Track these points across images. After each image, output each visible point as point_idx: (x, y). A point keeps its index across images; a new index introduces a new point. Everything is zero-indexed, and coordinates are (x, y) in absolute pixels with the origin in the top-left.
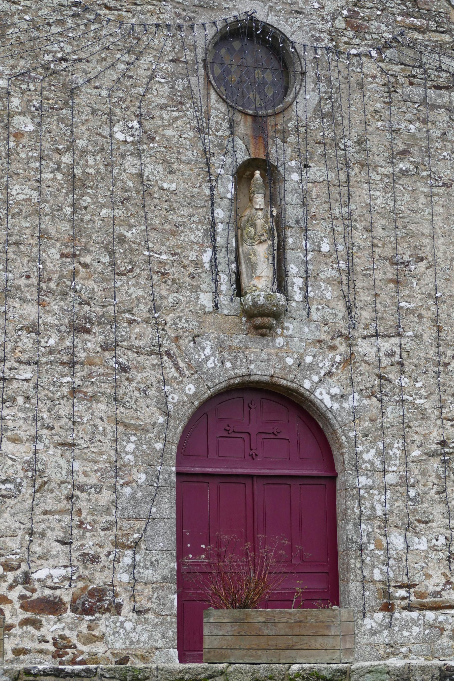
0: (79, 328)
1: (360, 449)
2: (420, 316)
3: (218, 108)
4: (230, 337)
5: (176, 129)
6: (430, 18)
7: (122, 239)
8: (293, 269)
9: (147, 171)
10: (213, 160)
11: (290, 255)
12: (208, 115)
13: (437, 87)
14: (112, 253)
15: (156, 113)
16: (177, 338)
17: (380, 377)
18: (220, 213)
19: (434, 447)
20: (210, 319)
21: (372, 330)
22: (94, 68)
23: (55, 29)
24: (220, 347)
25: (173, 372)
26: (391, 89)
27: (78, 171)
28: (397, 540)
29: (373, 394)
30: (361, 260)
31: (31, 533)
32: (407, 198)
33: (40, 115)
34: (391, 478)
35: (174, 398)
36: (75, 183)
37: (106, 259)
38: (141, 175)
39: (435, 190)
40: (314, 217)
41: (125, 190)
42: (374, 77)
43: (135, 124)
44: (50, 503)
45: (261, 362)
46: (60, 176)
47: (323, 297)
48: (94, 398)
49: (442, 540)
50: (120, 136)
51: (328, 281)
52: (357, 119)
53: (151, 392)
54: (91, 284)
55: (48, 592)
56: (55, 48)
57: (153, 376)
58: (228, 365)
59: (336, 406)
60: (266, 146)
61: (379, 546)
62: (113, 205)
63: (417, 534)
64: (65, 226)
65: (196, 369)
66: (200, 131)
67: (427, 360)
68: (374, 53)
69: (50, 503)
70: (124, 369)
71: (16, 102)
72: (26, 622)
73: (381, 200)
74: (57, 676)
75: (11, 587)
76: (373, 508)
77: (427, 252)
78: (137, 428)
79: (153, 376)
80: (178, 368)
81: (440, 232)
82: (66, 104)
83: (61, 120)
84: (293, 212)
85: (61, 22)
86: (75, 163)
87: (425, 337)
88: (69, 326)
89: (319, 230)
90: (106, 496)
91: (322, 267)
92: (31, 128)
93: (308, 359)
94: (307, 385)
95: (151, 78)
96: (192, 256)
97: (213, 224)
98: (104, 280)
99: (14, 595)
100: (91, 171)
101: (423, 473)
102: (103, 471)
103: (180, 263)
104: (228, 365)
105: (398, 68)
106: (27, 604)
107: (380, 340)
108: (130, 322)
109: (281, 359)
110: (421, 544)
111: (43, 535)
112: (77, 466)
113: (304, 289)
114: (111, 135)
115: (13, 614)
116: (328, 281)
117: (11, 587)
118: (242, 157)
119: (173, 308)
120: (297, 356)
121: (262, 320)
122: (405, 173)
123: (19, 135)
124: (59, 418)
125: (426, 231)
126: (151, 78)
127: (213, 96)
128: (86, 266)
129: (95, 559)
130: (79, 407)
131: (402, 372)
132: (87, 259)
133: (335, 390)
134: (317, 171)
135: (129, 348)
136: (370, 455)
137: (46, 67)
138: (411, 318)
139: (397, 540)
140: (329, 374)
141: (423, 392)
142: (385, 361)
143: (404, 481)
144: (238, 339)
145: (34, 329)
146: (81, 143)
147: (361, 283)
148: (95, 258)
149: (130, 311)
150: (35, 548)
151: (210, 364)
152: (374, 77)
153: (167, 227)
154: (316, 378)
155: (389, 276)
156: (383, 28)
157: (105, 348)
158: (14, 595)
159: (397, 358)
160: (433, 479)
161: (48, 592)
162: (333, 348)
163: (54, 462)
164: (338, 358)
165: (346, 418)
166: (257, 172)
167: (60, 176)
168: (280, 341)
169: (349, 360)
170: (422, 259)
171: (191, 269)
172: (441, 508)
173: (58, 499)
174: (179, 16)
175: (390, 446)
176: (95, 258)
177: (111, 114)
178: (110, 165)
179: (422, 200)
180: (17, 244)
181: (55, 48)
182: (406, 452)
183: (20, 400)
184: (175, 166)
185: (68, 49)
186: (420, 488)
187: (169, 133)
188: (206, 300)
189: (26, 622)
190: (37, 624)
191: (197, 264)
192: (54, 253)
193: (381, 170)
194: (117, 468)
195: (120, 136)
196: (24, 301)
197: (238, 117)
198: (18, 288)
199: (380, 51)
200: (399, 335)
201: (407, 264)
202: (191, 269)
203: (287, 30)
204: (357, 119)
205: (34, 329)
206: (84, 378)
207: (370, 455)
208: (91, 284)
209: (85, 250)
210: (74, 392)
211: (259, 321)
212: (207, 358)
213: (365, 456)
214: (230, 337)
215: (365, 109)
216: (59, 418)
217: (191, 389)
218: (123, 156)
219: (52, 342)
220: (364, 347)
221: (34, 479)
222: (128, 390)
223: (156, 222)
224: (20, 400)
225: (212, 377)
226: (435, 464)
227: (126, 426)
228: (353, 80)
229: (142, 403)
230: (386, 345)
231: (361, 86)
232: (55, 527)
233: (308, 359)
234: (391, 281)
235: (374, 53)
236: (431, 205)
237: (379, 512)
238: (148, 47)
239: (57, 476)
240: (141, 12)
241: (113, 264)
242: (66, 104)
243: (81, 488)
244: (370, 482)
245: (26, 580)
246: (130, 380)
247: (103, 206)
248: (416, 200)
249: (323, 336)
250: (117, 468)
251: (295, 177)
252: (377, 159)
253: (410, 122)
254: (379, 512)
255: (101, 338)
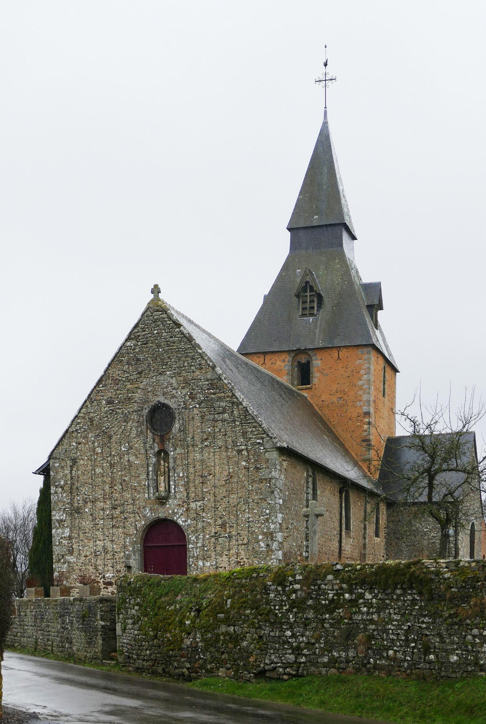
0: (114, 508)
1: (190, 536)
2: (210, 493)
3: (150, 434)
4: (154, 506)
5: (138, 445)
6: (217, 388)
7: (124, 480)
8: (171, 483)
9: (131, 459)
10: (149, 452)
11: (171, 479)
12: (147, 438)
13: (219, 414)
14: (122, 485)
15: (133, 440)
16: (140, 508)
17: (197, 514)
18: (150, 469)
19: (213, 534)
20: (148, 501)
21: (195, 500)
22: (116, 429)
23: (106, 419)
24: (151, 509)
25: (138, 518)
26: (202, 417)
27: (112, 462)
28: (200, 563)
29: (195, 519)
30: (192, 477)
31: (104, 565)
32: (207, 454)
33: (102, 447)
34: (199, 545)
35: (139, 525)
36: (112, 466)
37: (120, 487)
38: (129, 460)
39: (216, 450)
40: (178, 466)
41: (125, 466)
42: (197, 414)
43: (127, 445)
44: (109, 556)
45: (162, 513)
46: (108, 464)
47: (180, 491)
48: (118, 527)
49: (214, 562)
50: (123, 449)
51: (182, 485)
52: (191, 430)
53: (133, 524)
54: (117, 495)
55: (109, 580)
56: (106, 425)
57: (133, 520)
58: (153, 514)
59: (184, 524)
60: (163, 445)
61: (195, 565)
62: (121, 471)
63: (207, 561)
64: (110, 479)
65: (145, 516)
66: (145, 443)
67: (212, 507)
68: (197, 406)
69: (109, 557)
70: (126, 518)
71: (96, 444)
72: (104, 588)
73: (198, 456)
74: (235, 714)
75: (101, 579)
76: (194, 554)
77: (212, 472)
78: (129, 535)
79: (133, 520)
80: (140, 517)
81: (217, 464)
82: (109, 442)
83: (108, 447)
84: (171, 465)
85: (107, 416)
86: (111, 460)
87: (211, 500)
88: (112, 508)
89: (179, 469)
90: (122, 554)
91: (180, 481)
92: (100, 451)
93: (176, 510)
94: (175, 518)
95: (131, 429)
96: (143, 483)
97: (148, 473)
98: (120, 493)
99: (101, 581)
100: (116, 461)
101: (209, 543)
102: (121, 547)
103: (140, 485)
104: (153, 514)
105: (205, 409)
106: (105, 583)
107: (197, 503)
108: (127, 505)
109: (168, 511)
110: (208, 564)
111: (107, 565)
112: (114, 546)
113: (175, 489)
114: (121, 449)
115: (102, 586)
116: (182, 485)
117: (101, 579)
118: (156, 449)
119: (138, 499)
120: (174, 510)
121: (162, 501)
122: (206, 446)
123: (97, 454)
124: (110, 534)
125: (213, 465)
126: (131, 429)
127: (149, 431)
128: (115, 490)
129: (120, 571)
130: (115, 530)
131: (203, 512)
132: (116, 488)
133: (183, 519)
134: (178, 450)
135: (127, 512)
136: (193, 538)
137: (103, 432)
138: (207, 494)
139: (200, 563)
140: (182, 514)
141: (210, 517)
142: (199, 509)
143: (203, 546)
144: (156, 506)
145: (103, 509)
146: (113, 453)
147: (191, 485)
148: (118, 487)
149: (127, 502)
150: (106, 569)
151: (148, 515)
152: (197, 414)
153: (136, 475)
154: (178, 516)
155: (201, 481)
156: (201, 396)
157: (121, 513)
158: (101, 581)
159: (202, 508)
160: (212, 544)
161: (109, 580)
162: (183, 506)
163: (109, 545)
164: (184, 509)
165: (186, 527)
166: (162, 454)
167: (108, 464)
168: (168, 506)
169: (188, 510)
170: (211, 474)
171: (143, 487)
172: (214, 553)
173: (110, 556)
174: (139, 407)
175: (199, 535)
176: (118, 487)
177: (121, 442)
178: (120, 459)
179: (212, 454)
180: (98, 486)
181: (106, 425)
182: (204, 536)
183: (100, 530)
184: (138, 456)
185: (109, 424)
186: (208, 547)
187: (136, 446)
188: (146, 495)
189: (104, 588)
190: (107, 588)
191: (145, 485)
192: (107, 487)
193: (199, 446)
194: (125, 546)
195: (123, 449)
196: (101, 502)
197: (156, 437)
198: (99, 498)
199: (200, 405)
200: (203, 500)
201: (206, 477)
202: (143, 487)
203: (170, 404)
204: (191, 430)
205: (103, 509)
206: (116, 522)
207: (193, 538)
208: (117, 495)
209: (115, 485)
210: (113, 526)
211: (161, 501)
212: (148, 513)
213: (192, 539)
214: (154, 506)
215: (196, 429)
216: (110, 534)
217: (143, 522)
218: (124, 455)
219: (108, 513)
220: (193, 505)
221: (104, 551)
222: (127, 524)
223: (133, 474)
224: (100, 530)
225: (149, 519)
226: (213, 540)
227: (127, 534)
228: (191, 417)
229: (130, 528)
230: (199, 504)
231: (193, 418)
232: (110, 563)
233: (176, 510)
234: (201, 483)
235: (197, 406)
236: (214, 456)
237: (196, 555)
238: (130, 419)
239: (110, 549)
240: (129, 408)
241: (122, 488)
242: (109, 442)
243: (116, 552)
244: (193, 546)
245: (104, 577)
246: (127, 522)
247: (119, 471)
248: (209, 455)
249: (180, 503)
250: (125, 546)
251: (172, 453)
252: (198, 443)
253: (209, 428)
254: (196, 555)
255: (120, 510)
